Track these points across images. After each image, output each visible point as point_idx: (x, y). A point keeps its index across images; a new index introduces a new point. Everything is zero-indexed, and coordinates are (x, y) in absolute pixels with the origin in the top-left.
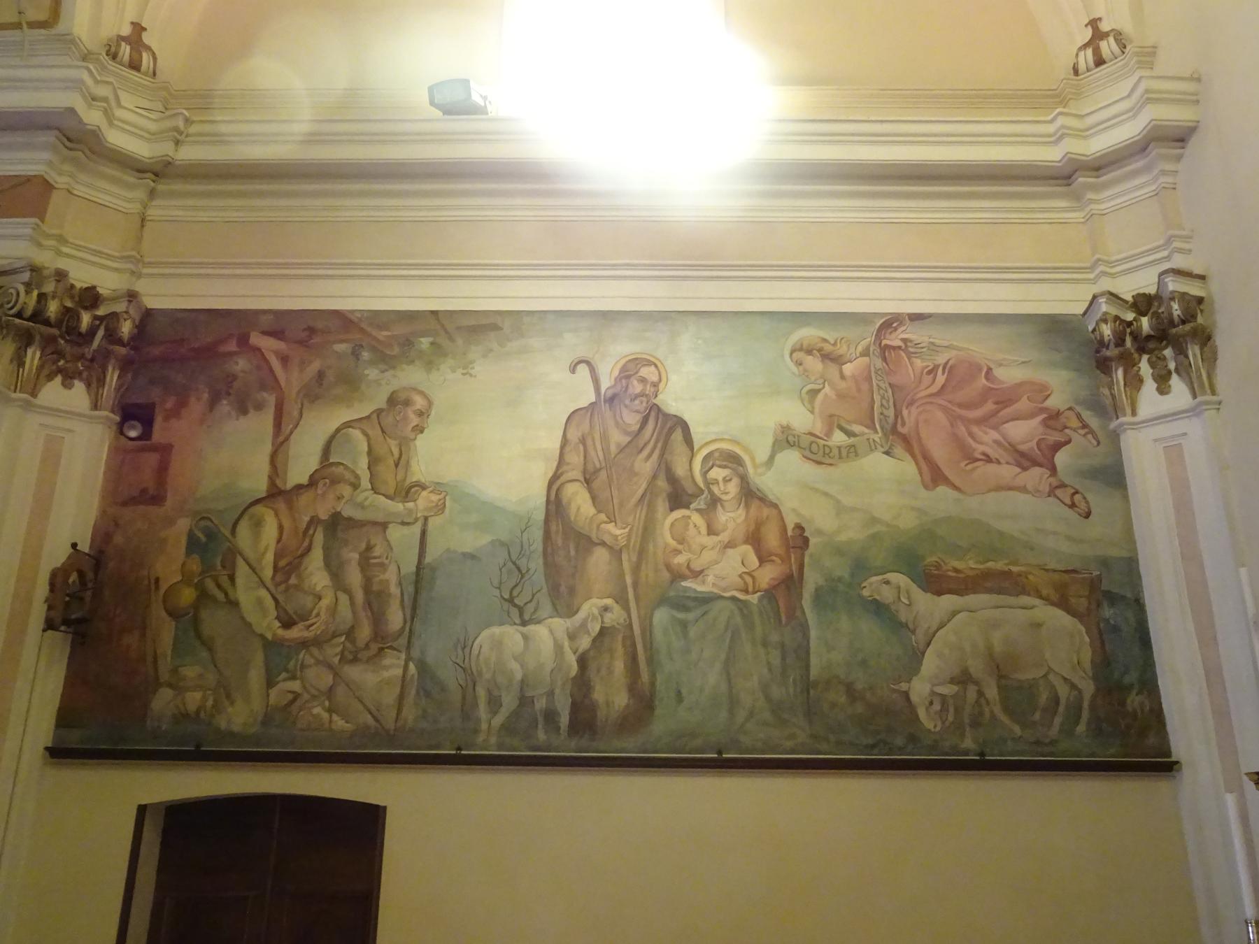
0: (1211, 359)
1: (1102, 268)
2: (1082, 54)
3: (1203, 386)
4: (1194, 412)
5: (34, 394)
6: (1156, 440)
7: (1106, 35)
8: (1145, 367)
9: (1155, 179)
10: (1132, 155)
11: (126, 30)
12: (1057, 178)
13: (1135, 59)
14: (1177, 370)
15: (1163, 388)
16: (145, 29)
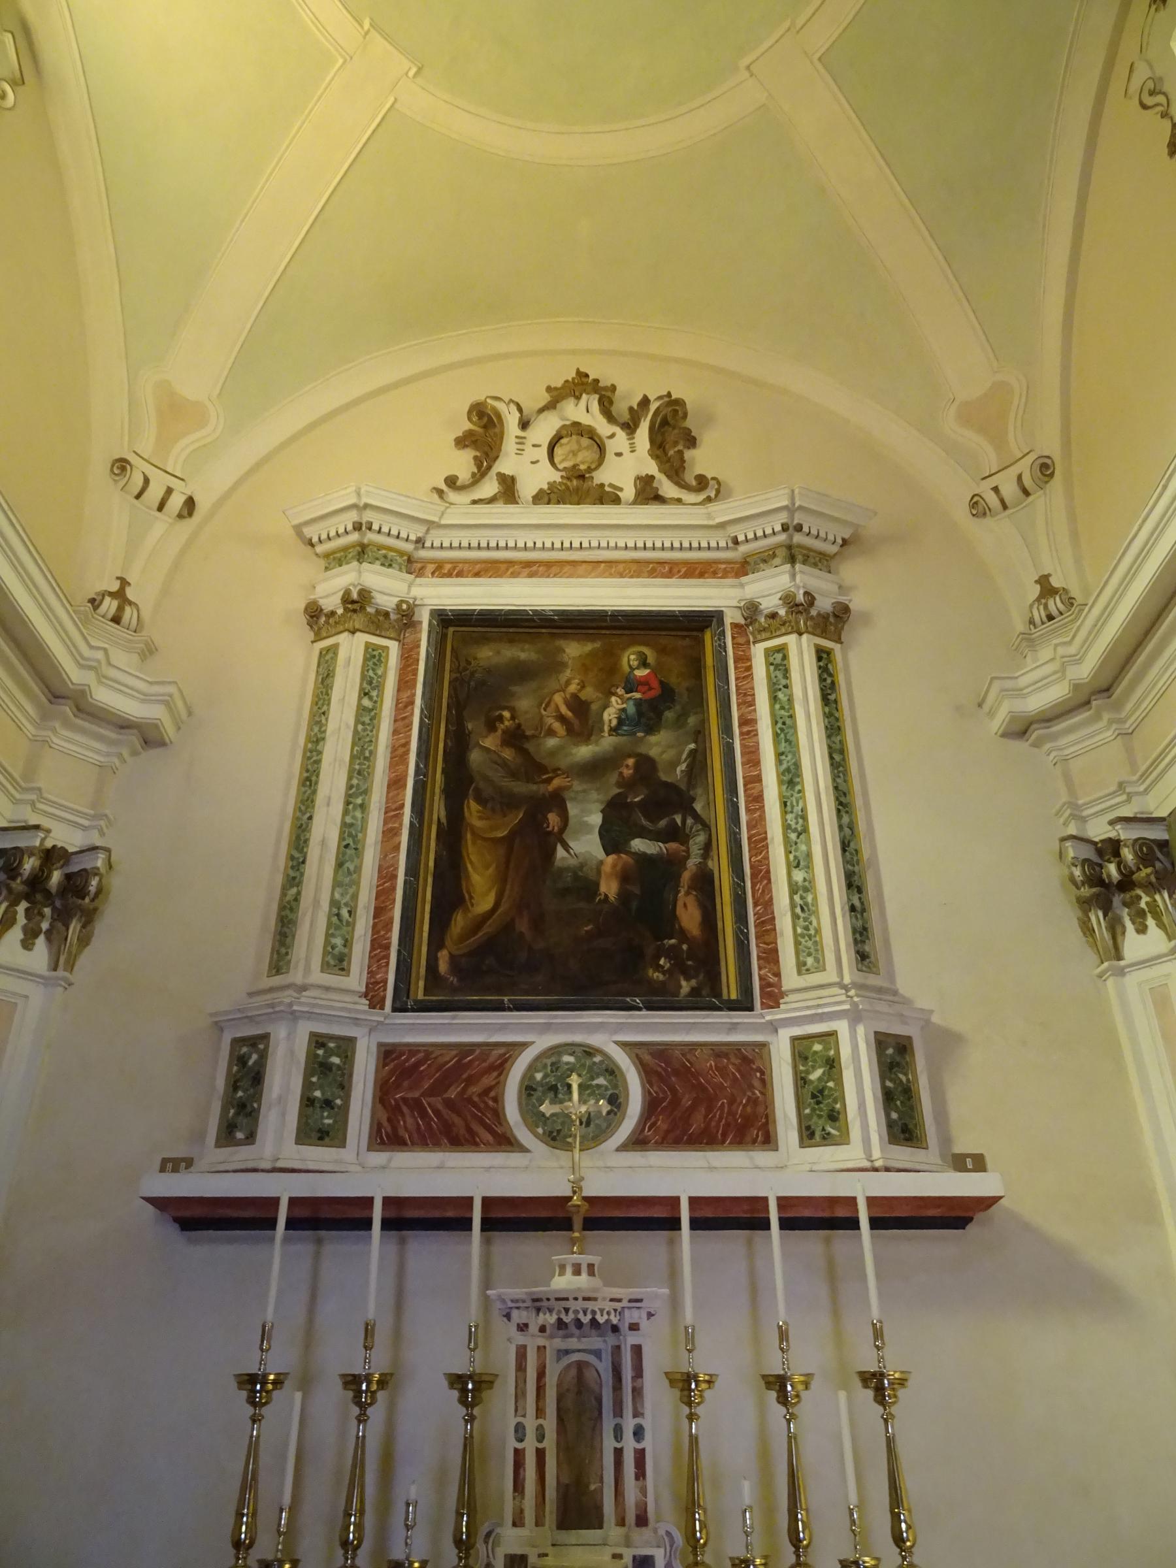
0: (84, 941)
3: (63, 958)
4: (46, 981)
5: (1119, 957)
9: (108, 755)
10: (109, 722)
12: (47, 687)
13: (142, 645)
14: (49, 934)
15: (27, 944)
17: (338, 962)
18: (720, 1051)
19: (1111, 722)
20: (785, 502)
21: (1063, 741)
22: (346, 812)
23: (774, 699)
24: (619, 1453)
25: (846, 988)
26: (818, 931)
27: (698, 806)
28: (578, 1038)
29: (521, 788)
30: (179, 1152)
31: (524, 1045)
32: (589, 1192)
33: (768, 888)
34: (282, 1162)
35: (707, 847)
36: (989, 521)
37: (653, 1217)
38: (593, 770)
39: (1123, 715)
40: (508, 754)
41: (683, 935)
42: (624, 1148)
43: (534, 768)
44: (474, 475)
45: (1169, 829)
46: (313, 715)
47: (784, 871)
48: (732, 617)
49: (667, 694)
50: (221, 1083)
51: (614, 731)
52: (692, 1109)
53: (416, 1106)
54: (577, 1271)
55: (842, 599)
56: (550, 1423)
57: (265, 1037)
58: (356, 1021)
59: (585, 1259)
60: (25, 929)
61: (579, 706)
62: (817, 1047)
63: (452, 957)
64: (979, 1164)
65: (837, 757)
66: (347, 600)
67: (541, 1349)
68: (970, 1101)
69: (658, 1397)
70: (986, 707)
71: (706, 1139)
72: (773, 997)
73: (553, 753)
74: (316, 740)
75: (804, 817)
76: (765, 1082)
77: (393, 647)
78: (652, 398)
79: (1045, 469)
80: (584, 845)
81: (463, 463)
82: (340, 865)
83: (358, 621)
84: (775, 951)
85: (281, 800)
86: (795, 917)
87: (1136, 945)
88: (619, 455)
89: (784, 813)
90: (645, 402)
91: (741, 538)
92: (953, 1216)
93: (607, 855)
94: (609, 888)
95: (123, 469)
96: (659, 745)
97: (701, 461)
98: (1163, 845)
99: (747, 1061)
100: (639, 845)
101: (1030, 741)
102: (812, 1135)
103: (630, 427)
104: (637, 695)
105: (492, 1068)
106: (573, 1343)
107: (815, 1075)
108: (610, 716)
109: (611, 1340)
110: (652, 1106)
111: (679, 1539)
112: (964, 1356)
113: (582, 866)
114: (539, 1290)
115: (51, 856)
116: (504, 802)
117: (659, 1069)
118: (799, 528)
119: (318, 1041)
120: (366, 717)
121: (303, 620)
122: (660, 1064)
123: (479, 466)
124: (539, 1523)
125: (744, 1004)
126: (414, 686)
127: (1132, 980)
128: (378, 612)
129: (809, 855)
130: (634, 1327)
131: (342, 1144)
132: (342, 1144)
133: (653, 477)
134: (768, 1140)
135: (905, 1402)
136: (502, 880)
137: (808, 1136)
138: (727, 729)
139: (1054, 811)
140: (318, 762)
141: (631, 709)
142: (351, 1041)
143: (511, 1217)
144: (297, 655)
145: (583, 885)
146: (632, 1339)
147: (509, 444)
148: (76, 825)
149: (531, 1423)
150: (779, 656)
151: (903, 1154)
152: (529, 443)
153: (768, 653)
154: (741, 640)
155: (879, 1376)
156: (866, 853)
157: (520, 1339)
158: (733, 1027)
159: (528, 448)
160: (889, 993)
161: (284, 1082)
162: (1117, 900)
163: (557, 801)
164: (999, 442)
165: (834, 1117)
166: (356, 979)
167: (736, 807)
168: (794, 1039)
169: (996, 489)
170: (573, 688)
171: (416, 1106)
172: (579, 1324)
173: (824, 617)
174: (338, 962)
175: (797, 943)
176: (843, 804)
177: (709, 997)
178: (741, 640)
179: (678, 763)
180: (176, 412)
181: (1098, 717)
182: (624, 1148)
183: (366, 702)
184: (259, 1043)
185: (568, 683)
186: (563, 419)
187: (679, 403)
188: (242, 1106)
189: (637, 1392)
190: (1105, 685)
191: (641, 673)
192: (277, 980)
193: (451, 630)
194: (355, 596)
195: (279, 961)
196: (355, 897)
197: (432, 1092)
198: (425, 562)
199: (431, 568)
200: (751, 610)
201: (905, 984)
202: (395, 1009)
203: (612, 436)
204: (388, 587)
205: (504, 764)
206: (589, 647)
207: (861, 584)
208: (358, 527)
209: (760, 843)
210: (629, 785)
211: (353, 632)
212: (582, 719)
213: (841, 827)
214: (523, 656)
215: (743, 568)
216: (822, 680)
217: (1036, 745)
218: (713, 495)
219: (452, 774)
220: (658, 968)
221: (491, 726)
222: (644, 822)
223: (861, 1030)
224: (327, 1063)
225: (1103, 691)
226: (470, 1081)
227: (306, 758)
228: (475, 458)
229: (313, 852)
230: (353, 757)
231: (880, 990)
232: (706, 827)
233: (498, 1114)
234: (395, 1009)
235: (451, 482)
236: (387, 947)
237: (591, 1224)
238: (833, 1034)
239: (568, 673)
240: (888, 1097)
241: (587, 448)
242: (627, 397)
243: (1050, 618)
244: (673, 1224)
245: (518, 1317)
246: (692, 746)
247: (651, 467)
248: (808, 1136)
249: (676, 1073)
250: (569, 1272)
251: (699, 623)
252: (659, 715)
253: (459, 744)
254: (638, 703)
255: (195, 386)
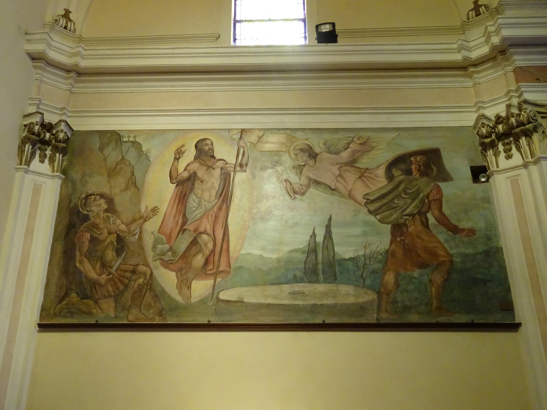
1: (479, 105)
2: (470, 13)
6: (507, 178)
7: (481, 6)
8: (501, 147)
11: (63, 12)
15: (509, 157)
16: (71, 12)
19: (71, 84)
21: (45, 74)
39: (76, 85)
45: (72, 135)
70: (28, 37)
87: (36, 164)
101: (34, 64)
117: (400, 211)
127: (29, 177)
139: (30, 97)
181: (67, 79)
217: (35, 67)
243: (66, 28)
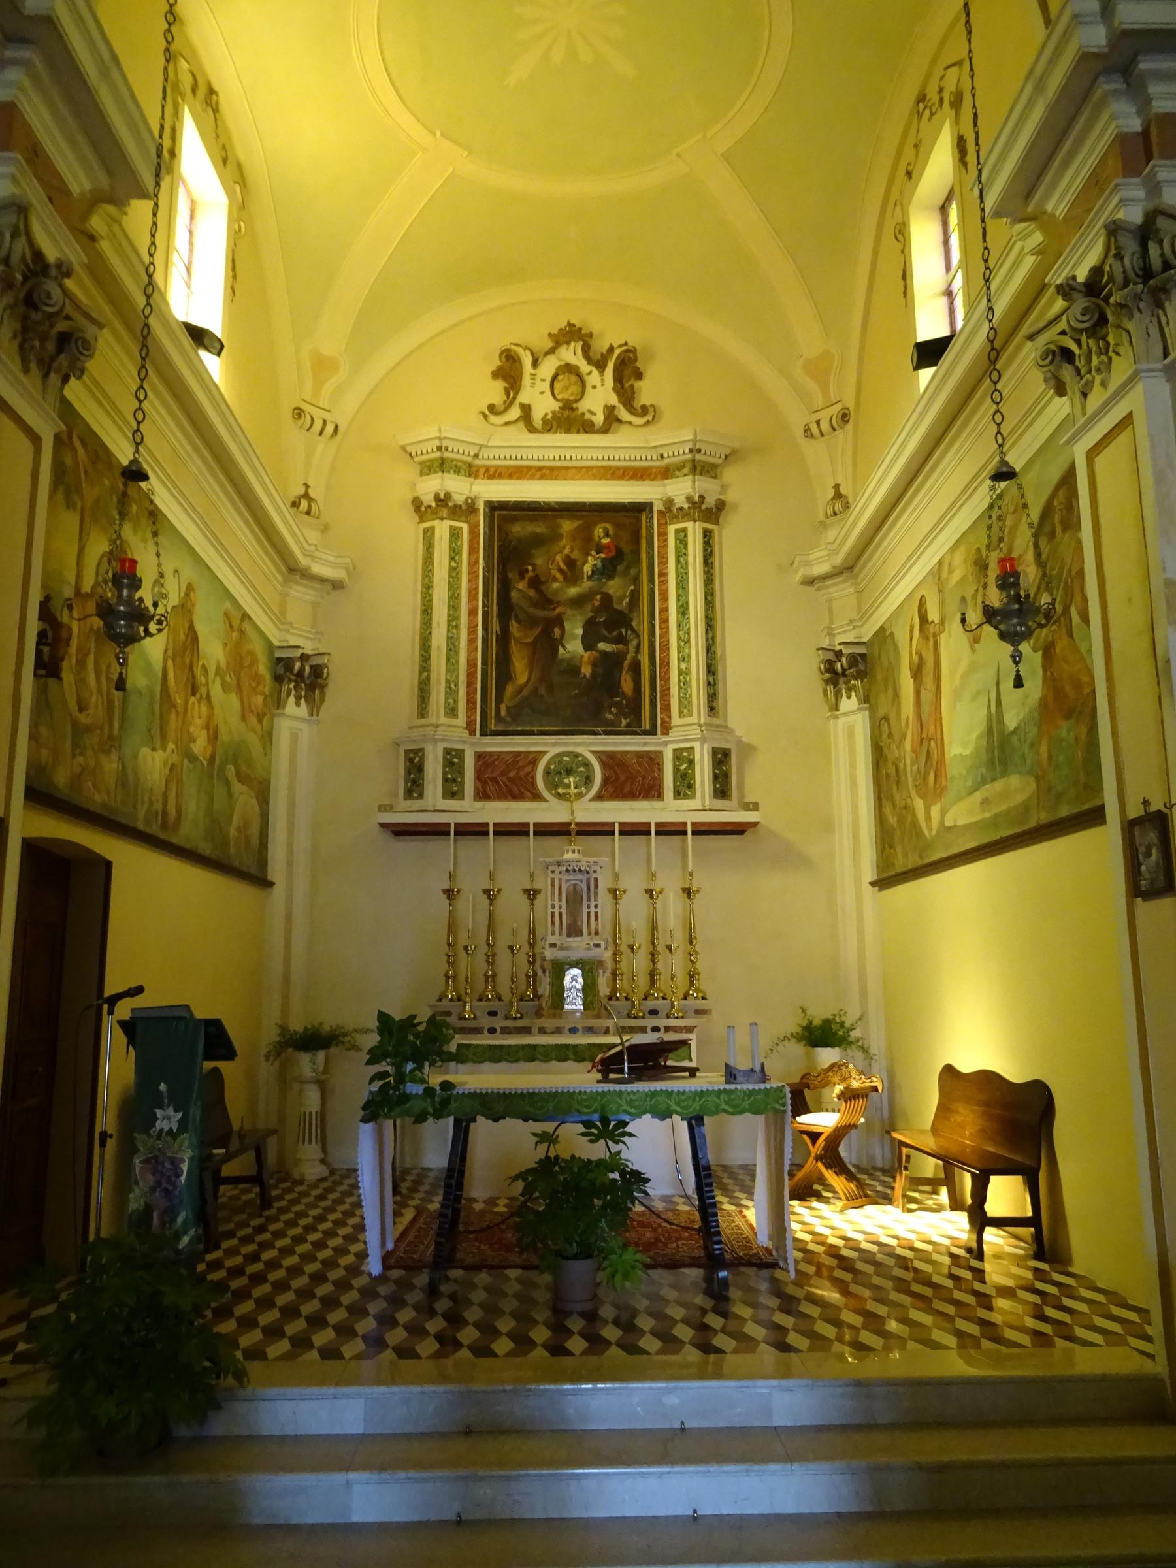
0: (322, 700)
4: (308, 722)
5: (837, 710)
15: (298, 704)
17: (452, 712)
18: (639, 755)
20: (691, 437)
21: (831, 590)
22: (448, 631)
23: (678, 562)
24: (589, 913)
25: (700, 726)
26: (690, 696)
27: (634, 624)
28: (571, 749)
29: (540, 613)
30: (387, 802)
31: (546, 752)
32: (577, 820)
33: (667, 672)
34: (434, 805)
35: (638, 647)
36: (813, 441)
37: (602, 830)
38: (578, 602)
40: (532, 593)
41: (624, 695)
42: (592, 800)
43: (546, 601)
44: (505, 402)
46: (424, 571)
47: (676, 662)
48: (658, 506)
49: (620, 554)
50: (402, 771)
51: (590, 578)
52: (625, 782)
53: (494, 780)
54: (573, 852)
55: (721, 497)
56: (564, 903)
57: (422, 750)
58: (464, 742)
59: (576, 848)
60: (296, 697)
61: (570, 562)
62: (685, 754)
63: (508, 709)
64: (755, 807)
65: (709, 598)
66: (437, 498)
67: (560, 880)
68: (753, 780)
69: (604, 898)
71: (631, 796)
72: (666, 729)
73: (556, 592)
74: (428, 587)
75: (688, 633)
76: (660, 769)
77: (465, 526)
78: (615, 345)
79: (845, 417)
80: (573, 646)
81: (495, 392)
82: (448, 660)
83: (445, 512)
84: (669, 705)
85: (410, 621)
86: (680, 688)
88: (594, 387)
89: (679, 630)
90: (611, 349)
91: (665, 455)
92: (738, 830)
93: (586, 650)
94: (586, 670)
95: (300, 415)
96: (615, 587)
97: (646, 392)
98: (863, 656)
99: (651, 759)
100: (602, 646)
102: (679, 794)
103: (601, 365)
104: (603, 555)
105: (530, 763)
106: (572, 877)
107: (683, 767)
108: (587, 569)
109: (586, 876)
110: (606, 781)
111: (610, 940)
112: (723, 882)
113: (572, 659)
114: (560, 859)
115: (304, 658)
116: (531, 622)
118: (699, 451)
119: (447, 752)
120: (454, 572)
121: (412, 509)
122: (610, 761)
123: (508, 395)
124: (560, 934)
125: (652, 732)
126: (478, 552)
127: (841, 721)
128: (455, 506)
129: (689, 655)
130: (595, 872)
131: (462, 798)
132: (462, 798)
133: (614, 407)
134: (660, 796)
135: (698, 900)
136: (531, 666)
137: (678, 794)
138: (651, 580)
140: (431, 600)
141: (599, 565)
142: (463, 751)
143: (546, 831)
144: (410, 530)
145: (573, 669)
146: (594, 875)
147: (526, 380)
148: (307, 638)
149: (557, 904)
150: (682, 535)
151: (719, 803)
152: (538, 378)
153: (677, 531)
154: (662, 522)
155: (689, 889)
156: (719, 653)
157: (551, 876)
158: (646, 744)
159: (538, 381)
160: (724, 728)
161: (434, 770)
162: (841, 680)
163: (559, 621)
164: (824, 386)
165: (690, 786)
166: (461, 720)
167: (653, 626)
168: (675, 750)
169: (818, 423)
170: (567, 551)
171: (494, 780)
172: (574, 871)
173: (709, 510)
174: (452, 712)
175: (680, 701)
176: (710, 626)
177: (635, 728)
178: (662, 522)
179: (625, 597)
180: (323, 366)
182: (592, 800)
183: (453, 564)
184: (419, 752)
185: (564, 548)
186: (560, 360)
187: (633, 351)
188: (414, 782)
189: (596, 894)
190: (850, 564)
191: (605, 541)
192: (423, 721)
193: (496, 513)
194: (442, 497)
195: (423, 712)
196: (457, 676)
197: (502, 774)
198: (479, 467)
199: (482, 471)
200: (669, 502)
201: (731, 723)
202: (481, 735)
203: (590, 373)
204: (460, 488)
205: (530, 598)
206: (576, 523)
207: (737, 485)
208: (439, 449)
209: (665, 647)
210: (597, 611)
211: (442, 519)
212: (572, 570)
213: (707, 640)
214: (538, 530)
215: (666, 473)
216: (705, 550)
218: (650, 418)
219: (503, 606)
220: (611, 713)
221: (522, 575)
222: (606, 633)
223: (706, 746)
224: (453, 761)
225: (848, 569)
226: (519, 769)
227: (423, 598)
228: (505, 388)
229: (434, 653)
230: (449, 598)
231: (718, 726)
232: (638, 636)
233: (533, 784)
234: (481, 735)
235: (492, 408)
236: (475, 703)
237: (579, 833)
238: (693, 748)
239: (563, 542)
240: (716, 777)
241: (575, 383)
242: (599, 347)
243: (835, 514)
244: (612, 833)
245: (551, 868)
246: (632, 587)
247: (614, 400)
248: (678, 794)
249: (618, 765)
250: (571, 852)
251: (642, 508)
252: (615, 568)
253: (505, 587)
254: (603, 560)
255: (330, 348)
